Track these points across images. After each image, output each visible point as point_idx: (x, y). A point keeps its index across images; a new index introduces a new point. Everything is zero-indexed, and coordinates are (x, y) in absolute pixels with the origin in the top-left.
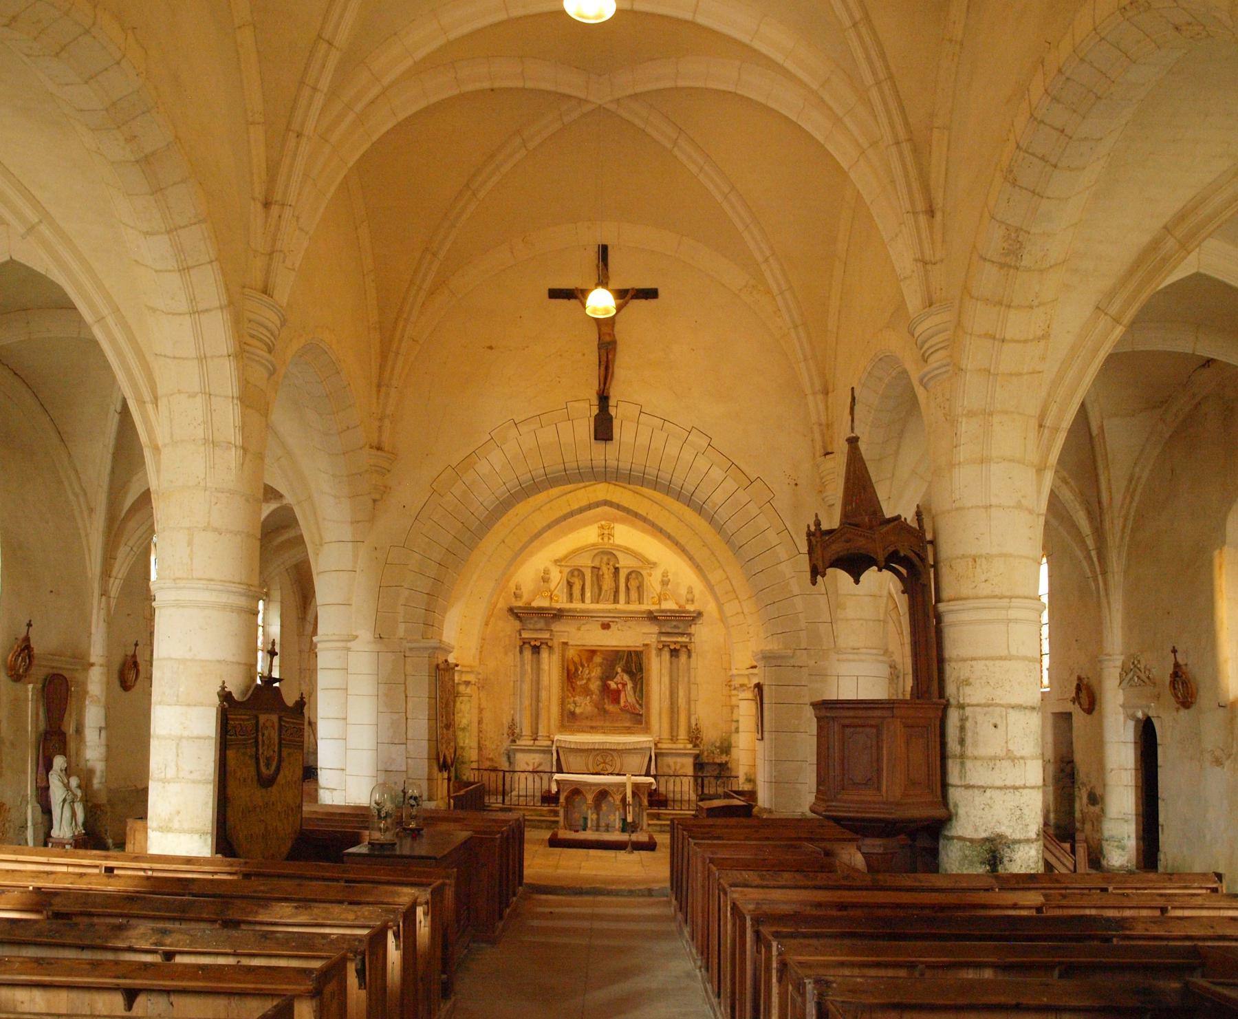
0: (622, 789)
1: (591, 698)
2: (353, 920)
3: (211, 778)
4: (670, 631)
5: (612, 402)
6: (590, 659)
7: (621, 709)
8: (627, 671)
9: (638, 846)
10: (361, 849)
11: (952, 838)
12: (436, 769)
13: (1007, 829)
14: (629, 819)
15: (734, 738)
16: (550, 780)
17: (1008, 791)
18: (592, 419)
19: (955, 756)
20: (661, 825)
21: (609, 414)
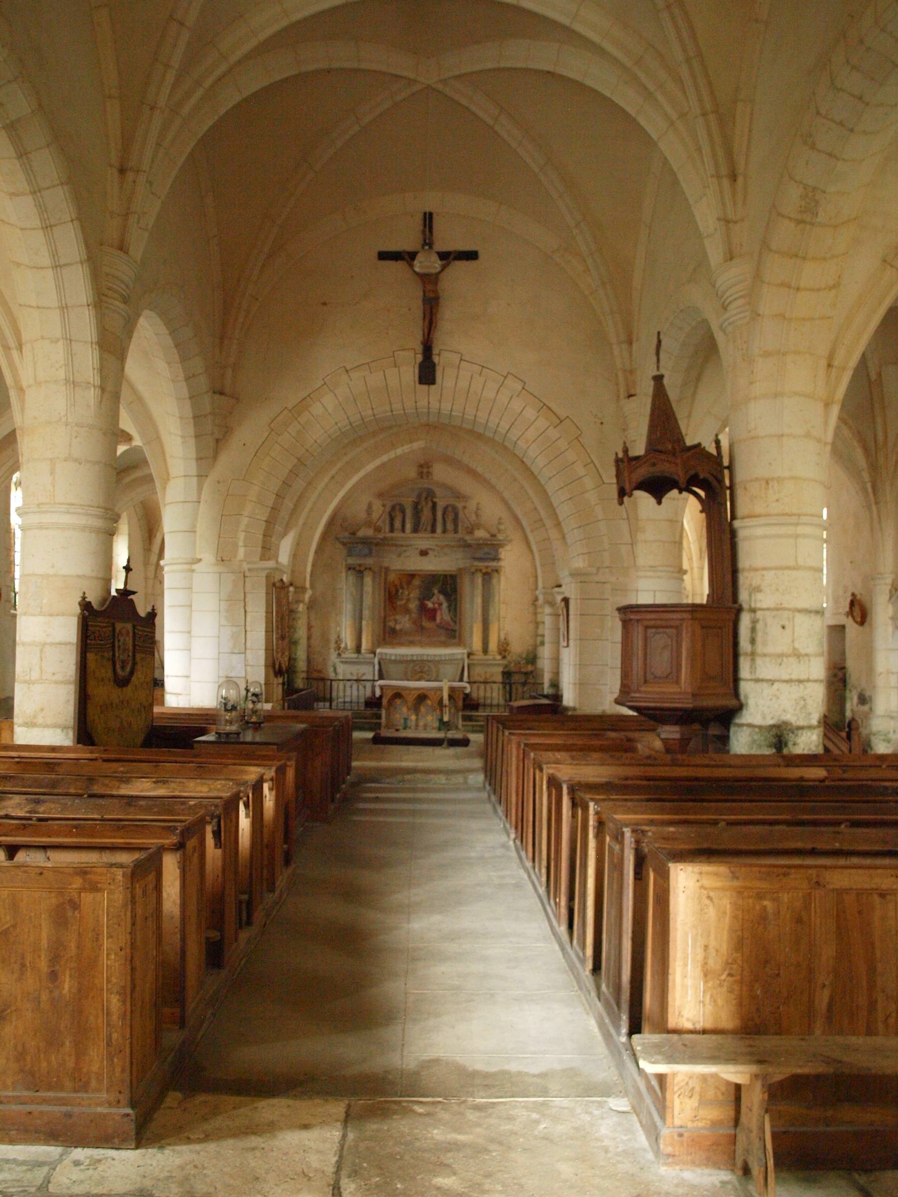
0: (438, 693)
2: (206, 793)
3: (73, 679)
4: (482, 556)
5: (435, 351)
6: (409, 583)
7: (437, 626)
9: (453, 743)
10: (210, 737)
11: (742, 725)
12: (272, 674)
13: (792, 717)
14: (446, 719)
16: (373, 687)
17: (793, 684)
18: (417, 366)
19: (746, 654)
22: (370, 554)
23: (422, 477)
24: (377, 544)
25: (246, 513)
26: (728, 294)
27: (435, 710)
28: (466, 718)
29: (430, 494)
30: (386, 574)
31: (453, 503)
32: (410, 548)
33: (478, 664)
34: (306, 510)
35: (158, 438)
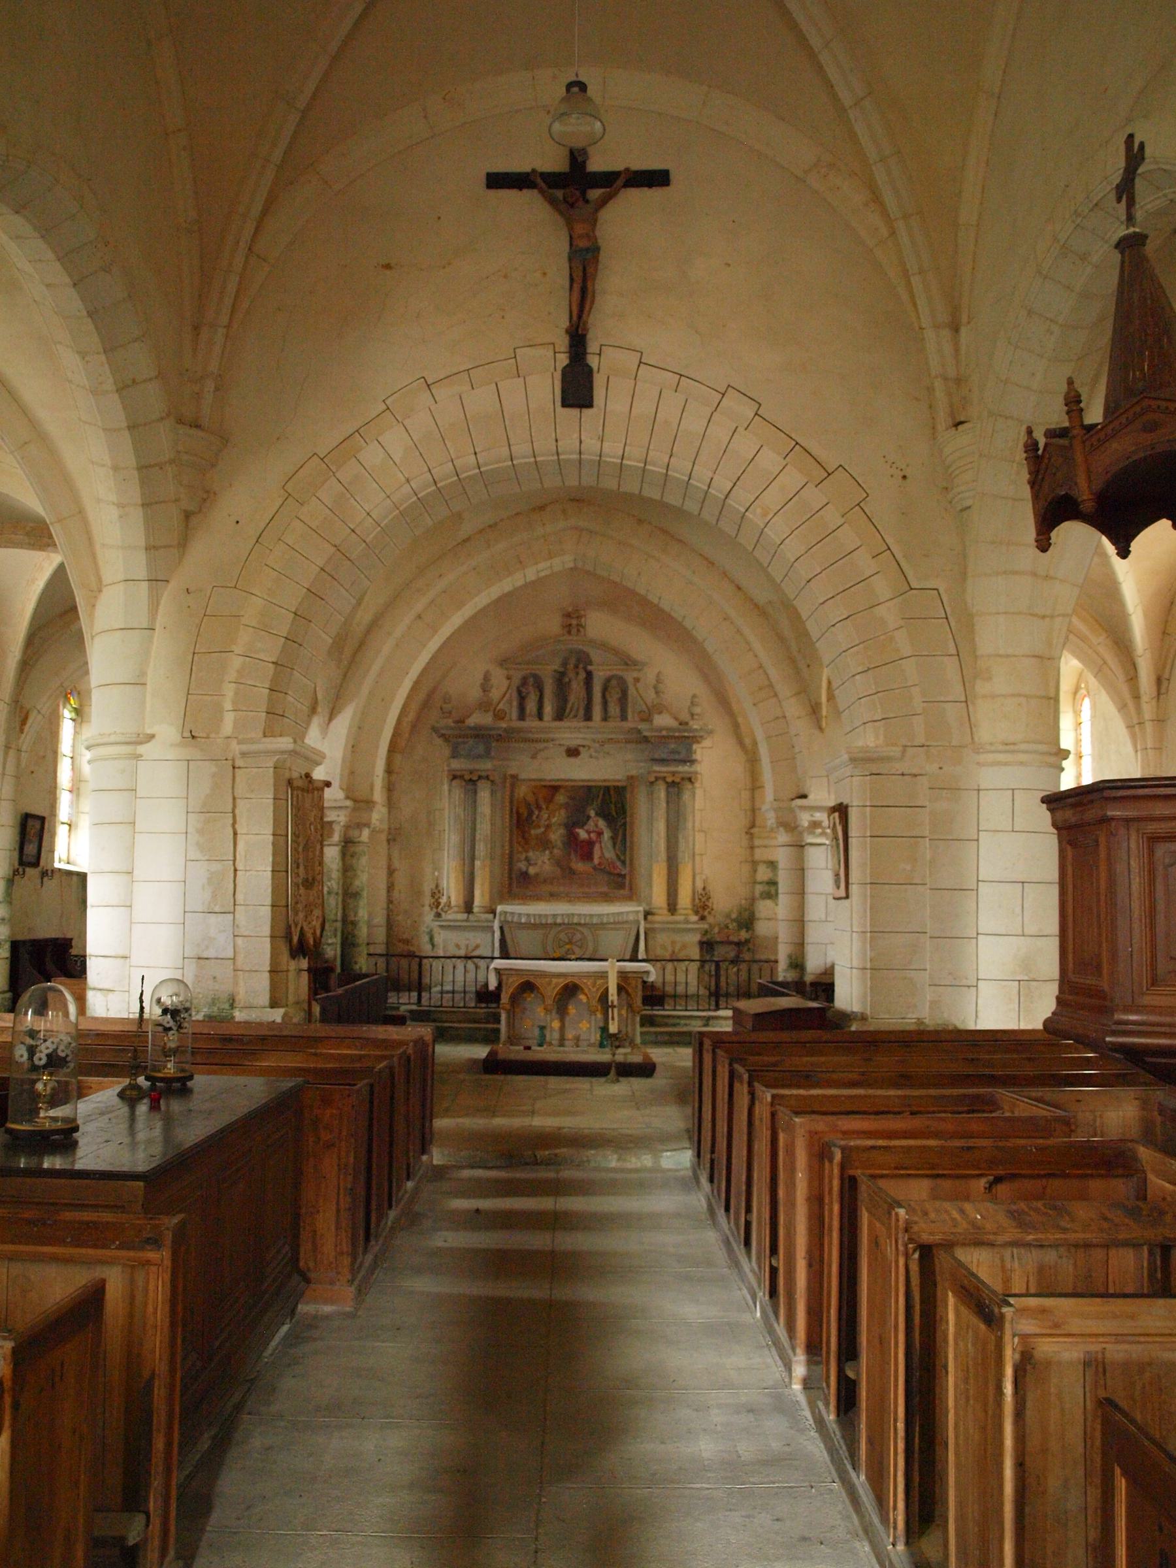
0: (599, 982)
1: (551, 853)
4: (664, 756)
5: (592, 347)
6: (550, 800)
7: (595, 868)
8: (604, 814)
9: (626, 1070)
14: (613, 1028)
15: (764, 908)
18: (558, 375)
20: (655, 1033)
21: (588, 366)
22: (487, 754)
23: (569, 632)
24: (499, 738)
25: (238, 649)
26: (954, 467)
27: (593, 1013)
28: (648, 1021)
29: (583, 660)
30: (513, 786)
31: (620, 673)
32: (550, 745)
33: (663, 930)
34: (376, 668)
35: (81, 512)
